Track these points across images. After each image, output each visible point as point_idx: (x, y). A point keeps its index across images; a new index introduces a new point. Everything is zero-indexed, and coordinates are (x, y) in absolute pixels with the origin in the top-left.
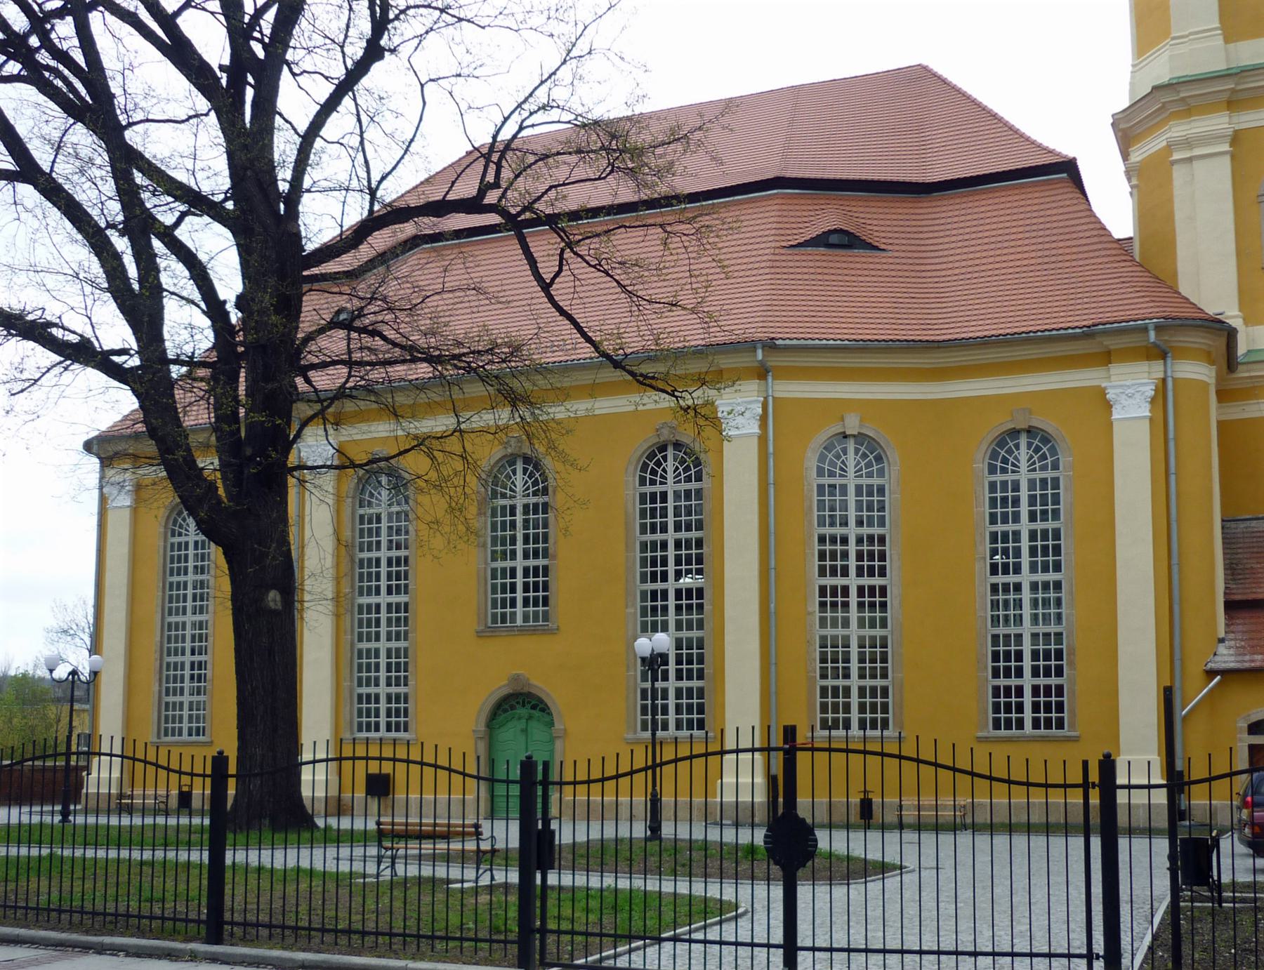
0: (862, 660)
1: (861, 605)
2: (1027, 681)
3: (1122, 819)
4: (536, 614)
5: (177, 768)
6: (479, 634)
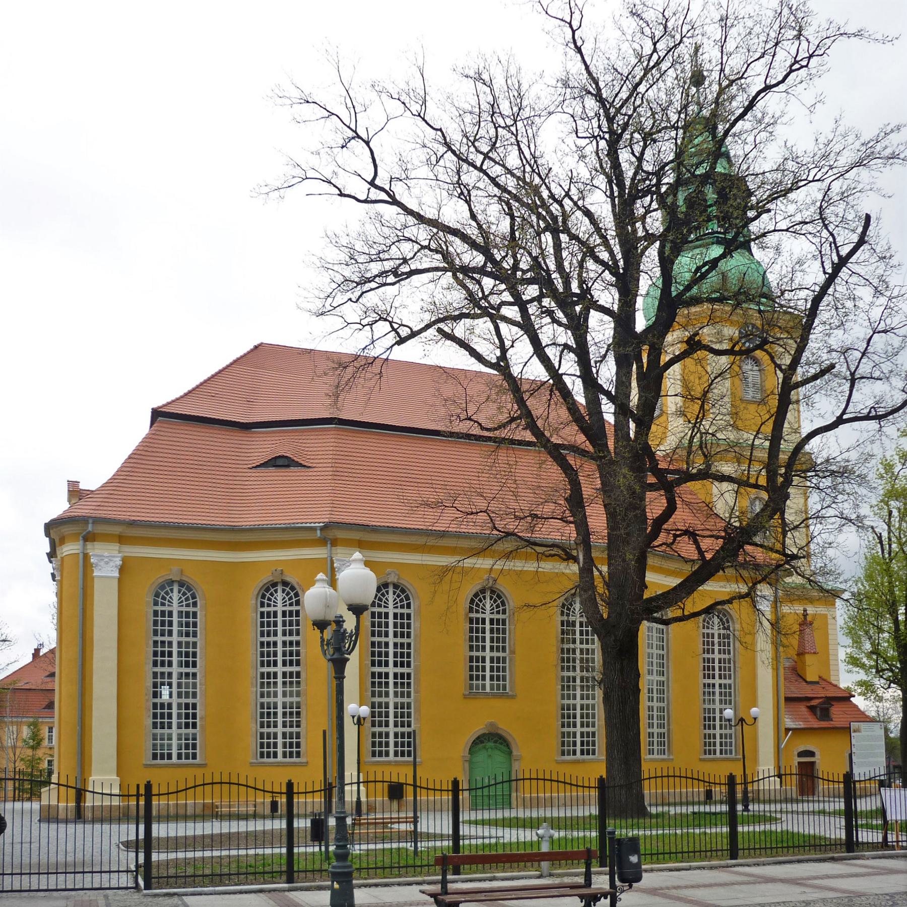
0: (396, 717)
1: (396, 684)
2: (391, 729)
3: (154, 812)
4: (498, 686)
5: (61, 787)
6: (465, 697)
